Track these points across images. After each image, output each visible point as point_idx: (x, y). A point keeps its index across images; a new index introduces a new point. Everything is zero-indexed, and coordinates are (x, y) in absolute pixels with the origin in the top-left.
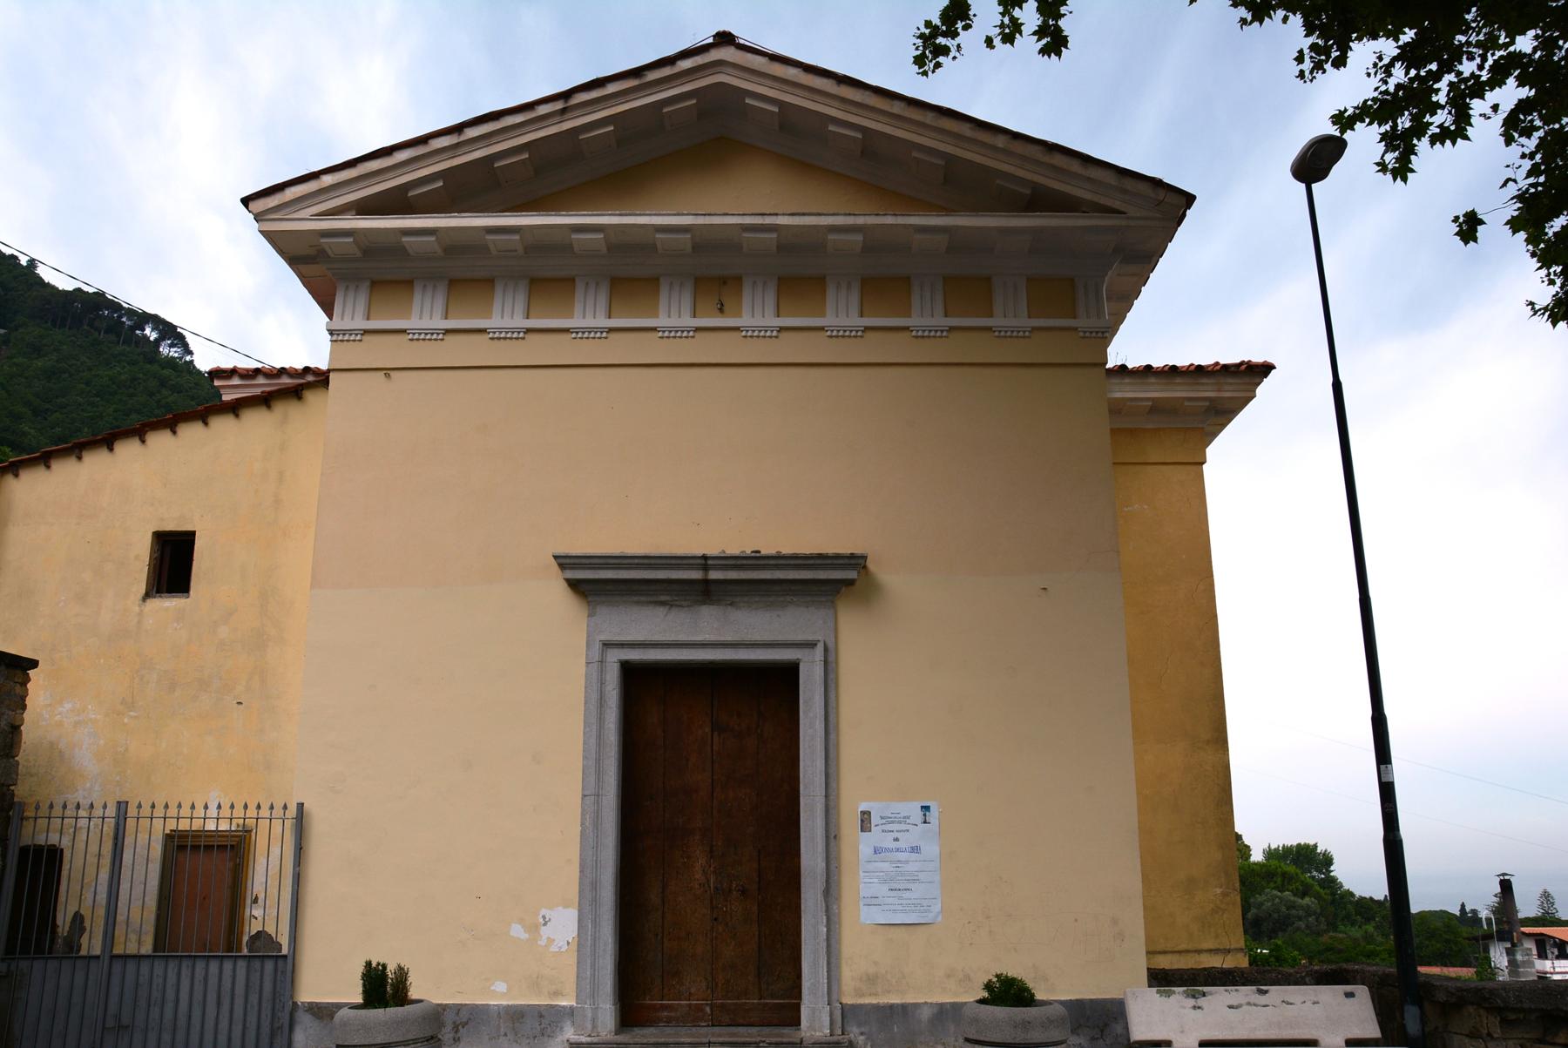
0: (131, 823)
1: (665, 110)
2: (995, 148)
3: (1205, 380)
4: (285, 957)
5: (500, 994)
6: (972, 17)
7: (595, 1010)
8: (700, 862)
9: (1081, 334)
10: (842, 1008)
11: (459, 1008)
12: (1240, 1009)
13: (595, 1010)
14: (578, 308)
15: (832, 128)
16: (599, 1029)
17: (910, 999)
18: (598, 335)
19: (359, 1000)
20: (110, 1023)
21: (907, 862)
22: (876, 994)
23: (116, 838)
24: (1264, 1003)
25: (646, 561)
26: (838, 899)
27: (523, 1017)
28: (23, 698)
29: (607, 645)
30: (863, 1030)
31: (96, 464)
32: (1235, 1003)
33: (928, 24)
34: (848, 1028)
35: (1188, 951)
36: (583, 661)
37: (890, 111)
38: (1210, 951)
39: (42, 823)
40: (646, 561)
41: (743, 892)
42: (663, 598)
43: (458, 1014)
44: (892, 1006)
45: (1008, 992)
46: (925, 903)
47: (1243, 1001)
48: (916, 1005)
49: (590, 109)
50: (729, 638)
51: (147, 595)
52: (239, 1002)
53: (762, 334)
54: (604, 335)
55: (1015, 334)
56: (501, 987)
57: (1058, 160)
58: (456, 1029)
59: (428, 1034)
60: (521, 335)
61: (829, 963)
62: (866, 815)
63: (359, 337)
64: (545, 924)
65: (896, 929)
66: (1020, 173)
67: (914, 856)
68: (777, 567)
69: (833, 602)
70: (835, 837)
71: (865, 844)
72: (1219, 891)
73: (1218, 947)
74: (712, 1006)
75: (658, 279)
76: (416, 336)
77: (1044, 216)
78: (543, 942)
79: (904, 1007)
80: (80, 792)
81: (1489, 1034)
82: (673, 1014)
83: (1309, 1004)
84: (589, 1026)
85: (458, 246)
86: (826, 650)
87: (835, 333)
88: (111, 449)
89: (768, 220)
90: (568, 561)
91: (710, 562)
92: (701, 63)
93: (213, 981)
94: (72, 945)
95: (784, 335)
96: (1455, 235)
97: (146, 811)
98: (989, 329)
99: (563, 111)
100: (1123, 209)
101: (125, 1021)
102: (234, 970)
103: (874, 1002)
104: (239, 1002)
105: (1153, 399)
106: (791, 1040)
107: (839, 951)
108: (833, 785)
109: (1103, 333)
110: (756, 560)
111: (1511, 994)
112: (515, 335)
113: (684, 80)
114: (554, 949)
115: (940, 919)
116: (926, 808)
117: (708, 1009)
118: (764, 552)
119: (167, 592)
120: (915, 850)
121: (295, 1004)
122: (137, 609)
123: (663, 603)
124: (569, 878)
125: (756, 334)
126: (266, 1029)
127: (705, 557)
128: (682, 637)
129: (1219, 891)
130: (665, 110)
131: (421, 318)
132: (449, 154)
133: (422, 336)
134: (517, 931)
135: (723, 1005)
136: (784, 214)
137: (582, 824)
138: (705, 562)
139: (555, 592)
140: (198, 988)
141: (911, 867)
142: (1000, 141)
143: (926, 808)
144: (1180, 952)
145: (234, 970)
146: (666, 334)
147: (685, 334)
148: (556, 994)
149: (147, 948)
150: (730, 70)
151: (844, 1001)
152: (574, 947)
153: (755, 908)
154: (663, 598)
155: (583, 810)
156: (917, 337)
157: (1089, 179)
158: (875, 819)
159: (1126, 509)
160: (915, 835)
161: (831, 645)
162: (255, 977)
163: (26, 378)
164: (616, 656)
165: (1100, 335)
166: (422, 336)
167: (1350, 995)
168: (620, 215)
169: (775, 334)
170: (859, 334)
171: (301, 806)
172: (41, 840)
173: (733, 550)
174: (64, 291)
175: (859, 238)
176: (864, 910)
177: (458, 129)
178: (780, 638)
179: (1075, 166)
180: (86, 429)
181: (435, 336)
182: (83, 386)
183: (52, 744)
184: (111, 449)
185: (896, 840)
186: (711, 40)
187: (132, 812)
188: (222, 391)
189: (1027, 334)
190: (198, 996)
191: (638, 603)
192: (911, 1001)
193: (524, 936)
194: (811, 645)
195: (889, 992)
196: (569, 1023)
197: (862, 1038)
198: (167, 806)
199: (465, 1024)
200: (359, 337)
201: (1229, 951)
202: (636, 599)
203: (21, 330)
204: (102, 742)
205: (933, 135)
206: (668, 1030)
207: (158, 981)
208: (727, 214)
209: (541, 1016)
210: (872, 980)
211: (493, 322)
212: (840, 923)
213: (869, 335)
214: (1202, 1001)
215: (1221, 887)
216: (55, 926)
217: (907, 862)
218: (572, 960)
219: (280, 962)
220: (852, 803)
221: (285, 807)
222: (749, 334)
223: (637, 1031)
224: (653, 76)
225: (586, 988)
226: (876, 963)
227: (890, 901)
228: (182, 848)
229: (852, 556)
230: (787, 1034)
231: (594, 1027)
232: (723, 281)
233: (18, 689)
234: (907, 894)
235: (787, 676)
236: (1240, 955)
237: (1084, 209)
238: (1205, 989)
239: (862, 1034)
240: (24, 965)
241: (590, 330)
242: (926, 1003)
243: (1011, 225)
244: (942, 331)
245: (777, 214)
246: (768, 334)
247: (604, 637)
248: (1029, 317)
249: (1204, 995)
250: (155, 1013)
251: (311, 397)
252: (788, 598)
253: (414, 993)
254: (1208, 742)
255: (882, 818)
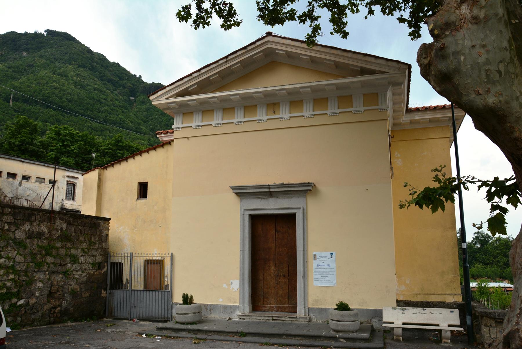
0: (134, 258)
1: (254, 57)
2: (348, 57)
3: (446, 111)
4: (170, 291)
5: (221, 302)
6: (6, 260)
7: (244, 307)
8: (273, 268)
9: (379, 110)
10: (308, 309)
11: (211, 305)
12: (416, 314)
13: (244, 307)
14: (236, 116)
15: (301, 56)
16: (245, 312)
17: (327, 307)
18: (241, 123)
19: (182, 302)
20: (132, 305)
21: (326, 269)
22: (318, 305)
23: (130, 262)
24: (424, 313)
25: (253, 187)
26: (307, 279)
27: (226, 308)
28: (108, 228)
29: (245, 210)
30: (314, 315)
31: (124, 164)
32: (415, 312)
33: (308, 34)
34: (310, 314)
35: (442, 294)
36: (239, 215)
37: (316, 49)
38: (449, 294)
39: (117, 258)
40: (253, 187)
41: (284, 276)
42: (260, 197)
43: (211, 307)
44: (322, 309)
45: (342, 307)
46: (331, 280)
47: (418, 312)
48: (329, 309)
49: (233, 60)
50: (277, 207)
51: (138, 199)
52: (160, 302)
53: (285, 119)
54: (243, 123)
55: (359, 112)
56: (221, 300)
57: (367, 58)
58: (210, 310)
59: (197, 311)
60: (221, 125)
61: (304, 296)
62: (315, 256)
63: (180, 129)
64: (232, 284)
65: (323, 287)
66: (356, 64)
67: (328, 267)
68: (288, 187)
69: (305, 196)
70: (306, 262)
71: (315, 263)
72: (452, 275)
73: (452, 293)
74: (276, 307)
75: (257, 105)
76: (195, 128)
77: (364, 77)
78: (231, 289)
79: (325, 309)
80: (126, 249)
81: (491, 325)
82: (266, 308)
83: (438, 314)
84: (242, 311)
85: (202, 102)
86: (303, 209)
87: (306, 117)
88: (127, 161)
89: (283, 87)
90: (233, 188)
91: (270, 187)
92: (262, 42)
93: (154, 297)
94: (126, 286)
95: (291, 119)
96: (179, 10)
97: (137, 255)
98: (351, 112)
99: (226, 62)
100: (388, 72)
101: (136, 305)
102: (158, 294)
103: (317, 307)
104: (160, 302)
105: (429, 119)
106: (293, 316)
107: (308, 293)
108: (306, 247)
109: (386, 109)
110: (283, 185)
111: (496, 314)
112: (220, 125)
113: (258, 48)
114: (234, 290)
115: (336, 285)
116: (332, 254)
117: (275, 307)
118: (285, 183)
119: (143, 198)
120: (329, 265)
121: (173, 303)
122: (135, 203)
123: (260, 198)
124: (237, 272)
125: (283, 119)
126: (166, 309)
127: (269, 185)
128: (264, 207)
129: (452, 275)
130: (254, 57)
131: (196, 123)
132: (198, 78)
133: (196, 128)
134: (225, 286)
135: (279, 306)
136: (287, 85)
137: (240, 258)
138: (269, 187)
139: (232, 196)
140: (151, 298)
141: (328, 270)
142: (350, 55)
143: (332, 254)
144: (439, 294)
145: (158, 294)
146: (259, 121)
147: (264, 121)
148: (235, 302)
149: (142, 288)
150: (271, 43)
151: (309, 307)
152: (239, 290)
153: (287, 281)
154: (260, 197)
155: (240, 254)
156: (329, 116)
157: (377, 63)
158: (317, 257)
159: (422, 154)
160: (329, 261)
161: (305, 208)
162: (163, 296)
163: (141, 112)
164: (247, 213)
165: (385, 110)
166: (196, 128)
167: (452, 312)
168: (243, 90)
169: (289, 119)
170: (313, 116)
171: (172, 253)
172: (117, 261)
173: (277, 183)
174: (149, 84)
175: (309, 89)
176: (315, 282)
177: (199, 70)
178: (291, 206)
179: (373, 60)
180: (159, 126)
181: (199, 127)
182: (157, 112)
183: (119, 237)
184: (127, 161)
185: (324, 263)
186: (265, 35)
187: (134, 255)
188: (160, 138)
189: (363, 112)
190: (151, 300)
191: (253, 198)
192: (328, 307)
193: (226, 287)
194: (299, 208)
195: (321, 305)
196: (238, 310)
197: (314, 317)
198: (141, 254)
199: (212, 309)
200: (180, 129)
201: (455, 295)
202: (253, 197)
203: (139, 97)
204: (130, 237)
205: (329, 55)
206: (264, 313)
207: (142, 296)
208: (271, 87)
209: (231, 308)
210: (317, 301)
211: (214, 122)
212: (308, 285)
213: (316, 117)
214: (405, 311)
215: (453, 274)
216: (122, 282)
217: (326, 269)
218: (238, 294)
219: (169, 292)
220: (312, 252)
221: (168, 254)
222: (282, 119)
223: (256, 312)
224: (249, 48)
225: (242, 301)
226: (318, 297)
227: (321, 279)
228: (148, 263)
229: (309, 183)
230: (294, 315)
231: (244, 311)
232: (275, 104)
233: (107, 226)
234: (326, 278)
235: (292, 218)
236: (459, 296)
237: (377, 73)
238: (407, 308)
239: (314, 316)
240: (114, 291)
241: (239, 122)
242: (332, 308)
243: (353, 81)
244: (337, 114)
245: (285, 85)
246: (287, 119)
247: (244, 208)
248: (364, 107)
249: (406, 310)
250: (142, 303)
251: (166, 147)
252: (293, 195)
253: (195, 301)
254: (449, 228)
255: (319, 256)
